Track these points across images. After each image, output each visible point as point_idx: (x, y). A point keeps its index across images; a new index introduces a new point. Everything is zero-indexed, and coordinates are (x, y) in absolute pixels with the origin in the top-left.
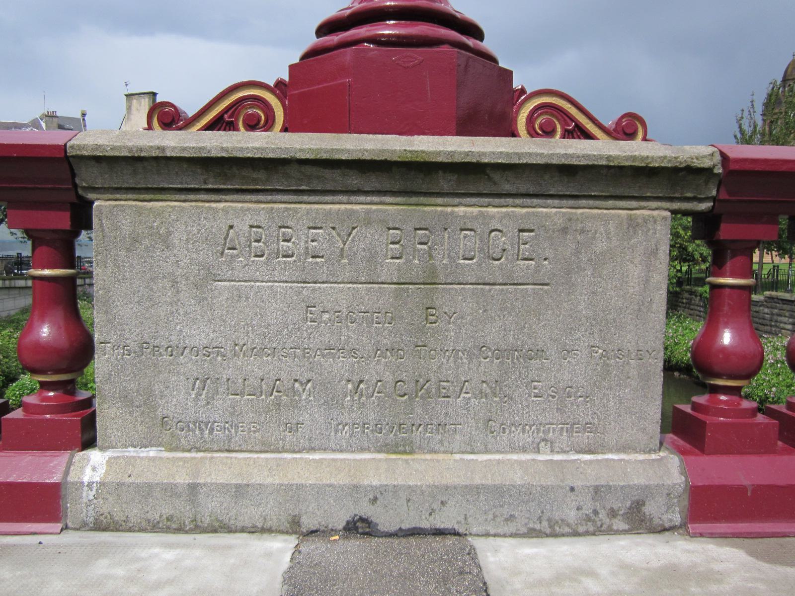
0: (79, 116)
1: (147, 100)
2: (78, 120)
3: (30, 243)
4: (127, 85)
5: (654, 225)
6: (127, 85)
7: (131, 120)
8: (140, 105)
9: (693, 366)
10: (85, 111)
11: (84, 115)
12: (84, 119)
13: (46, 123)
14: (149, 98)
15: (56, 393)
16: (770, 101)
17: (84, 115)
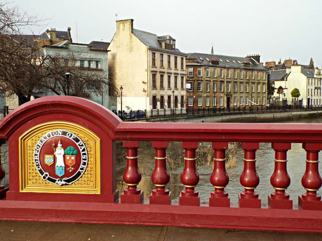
0: (66, 30)
3: (63, 149)
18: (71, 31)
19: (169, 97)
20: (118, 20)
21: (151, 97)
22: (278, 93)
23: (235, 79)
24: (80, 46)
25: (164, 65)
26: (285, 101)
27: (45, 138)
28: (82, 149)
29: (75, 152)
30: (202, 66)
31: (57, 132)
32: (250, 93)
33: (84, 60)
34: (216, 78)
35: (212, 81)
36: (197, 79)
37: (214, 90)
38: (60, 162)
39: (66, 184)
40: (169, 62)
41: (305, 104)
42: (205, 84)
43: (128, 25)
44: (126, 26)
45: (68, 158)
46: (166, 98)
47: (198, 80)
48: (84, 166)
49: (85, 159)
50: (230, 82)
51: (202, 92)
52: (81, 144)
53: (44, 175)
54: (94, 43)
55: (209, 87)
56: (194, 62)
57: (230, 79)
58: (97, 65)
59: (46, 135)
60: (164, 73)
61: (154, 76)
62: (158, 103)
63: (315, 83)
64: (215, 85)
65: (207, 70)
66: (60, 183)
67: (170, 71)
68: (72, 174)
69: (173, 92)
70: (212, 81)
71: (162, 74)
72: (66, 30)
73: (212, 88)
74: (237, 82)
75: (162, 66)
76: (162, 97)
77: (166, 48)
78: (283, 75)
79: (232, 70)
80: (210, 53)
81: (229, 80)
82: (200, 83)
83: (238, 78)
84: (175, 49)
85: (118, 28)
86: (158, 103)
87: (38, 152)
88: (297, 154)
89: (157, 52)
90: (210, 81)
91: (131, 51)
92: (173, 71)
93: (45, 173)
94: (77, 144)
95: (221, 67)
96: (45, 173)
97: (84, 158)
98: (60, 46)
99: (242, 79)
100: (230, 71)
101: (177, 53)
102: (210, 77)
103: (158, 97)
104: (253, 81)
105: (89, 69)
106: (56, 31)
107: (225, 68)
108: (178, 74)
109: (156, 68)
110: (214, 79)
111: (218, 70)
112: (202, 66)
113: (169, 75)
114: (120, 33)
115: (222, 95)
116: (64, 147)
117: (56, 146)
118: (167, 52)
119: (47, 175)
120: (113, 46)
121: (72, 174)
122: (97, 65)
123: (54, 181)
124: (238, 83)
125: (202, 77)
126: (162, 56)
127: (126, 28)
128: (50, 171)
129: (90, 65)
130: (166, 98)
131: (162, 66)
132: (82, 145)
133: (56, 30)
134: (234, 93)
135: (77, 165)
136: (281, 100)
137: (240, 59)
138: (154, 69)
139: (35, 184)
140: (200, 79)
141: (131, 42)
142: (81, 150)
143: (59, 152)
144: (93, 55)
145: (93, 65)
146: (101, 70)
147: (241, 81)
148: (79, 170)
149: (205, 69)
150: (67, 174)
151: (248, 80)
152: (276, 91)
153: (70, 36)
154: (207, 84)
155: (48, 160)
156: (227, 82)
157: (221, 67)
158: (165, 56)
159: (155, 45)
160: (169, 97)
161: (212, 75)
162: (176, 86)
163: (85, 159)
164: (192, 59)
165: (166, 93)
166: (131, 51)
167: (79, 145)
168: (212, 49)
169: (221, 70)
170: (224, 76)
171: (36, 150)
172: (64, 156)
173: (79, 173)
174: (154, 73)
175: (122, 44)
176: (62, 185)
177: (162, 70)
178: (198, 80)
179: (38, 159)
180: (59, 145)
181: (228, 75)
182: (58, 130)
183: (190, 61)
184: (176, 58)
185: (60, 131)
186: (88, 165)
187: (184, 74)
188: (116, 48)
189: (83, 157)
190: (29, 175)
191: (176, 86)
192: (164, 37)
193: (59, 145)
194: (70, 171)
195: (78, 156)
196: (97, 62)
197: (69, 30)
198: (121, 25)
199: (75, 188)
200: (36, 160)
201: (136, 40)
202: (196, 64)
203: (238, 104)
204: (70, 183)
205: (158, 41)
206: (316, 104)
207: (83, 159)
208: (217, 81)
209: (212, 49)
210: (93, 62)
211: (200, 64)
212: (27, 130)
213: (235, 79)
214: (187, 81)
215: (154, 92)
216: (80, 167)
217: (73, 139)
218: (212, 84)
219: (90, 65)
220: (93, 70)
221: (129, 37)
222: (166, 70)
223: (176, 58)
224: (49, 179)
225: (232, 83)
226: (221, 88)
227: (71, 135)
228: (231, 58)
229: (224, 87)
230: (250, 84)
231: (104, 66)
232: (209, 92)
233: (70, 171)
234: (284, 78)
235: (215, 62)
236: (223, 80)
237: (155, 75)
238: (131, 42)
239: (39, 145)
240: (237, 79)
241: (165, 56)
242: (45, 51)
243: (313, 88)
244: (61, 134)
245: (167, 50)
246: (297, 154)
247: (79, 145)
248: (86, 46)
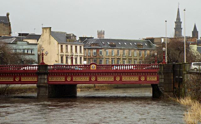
0: (6, 15)
12: (8, 17)
18: (9, 16)
23: (129, 57)
30: (103, 48)
33: (25, 50)
35: (110, 58)
36: (99, 57)
42: (105, 61)
43: (48, 30)
47: (99, 58)
50: (125, 59)
56: (97, 46)
58: (32, 52)
61: (62, 58)
65: (107, 51)
70: (110, 58)
72: (6, 15)
75: (67, 52)
79: (127, 50)
81: (125, 58)
82: (101, 60)
85: (43, 32)
88: (37, 67)
90: (109, 58)
91: (50, 44)
95: (117, 49)
99: (135, 57)
102: (108, 56)
105: (28, 54)
108: (77, 56)
110: (112, 57)
111: (115, 51)
112: (103, 48)
118: (70, 44)
120: (41, 41)
122: (32, 52)
124: (133, 60)
125: (103, 56)
127: (47, 32)
129: (28, 51)
138: (62, 54)
140: (101, 57)
141: (50, 39)
145: (29, 52)
146: (34, 54)
147: (135, 58)
149: (105, 50)
151: (142, 57)
153: (9, 20)
156: (123, 59)
159: (64, 39)
161: (110, 54)
164: (95, 44)
166: (50, 44)
168: (178, 9)
170: (120, 55)
174: (62, 56)
177: (67, 54)
178: (99, 58)
183: (94, 45)
187: (82, 56)
188: (42, 42)
192: (70, 35)
197: (8, 15)
198: (45, 30)
201: (52, 39)
202: (98, 47)
205: (67, 37)
208: (115, 58)
210: (30, 50)
211: (101, 47)
213: (129, 57)
214: (85, 59)
219: (28, 51)
220: (29, 54)
221: (49, 37)
222: (65, 54)
225: (127, 60)
231: (35, 52)
235: (113, 44)
236: (119, 57)
237: (62, 57)
238: (50, 39)
240: (131, 57)
245: (70, 43)
246: (37, 67)
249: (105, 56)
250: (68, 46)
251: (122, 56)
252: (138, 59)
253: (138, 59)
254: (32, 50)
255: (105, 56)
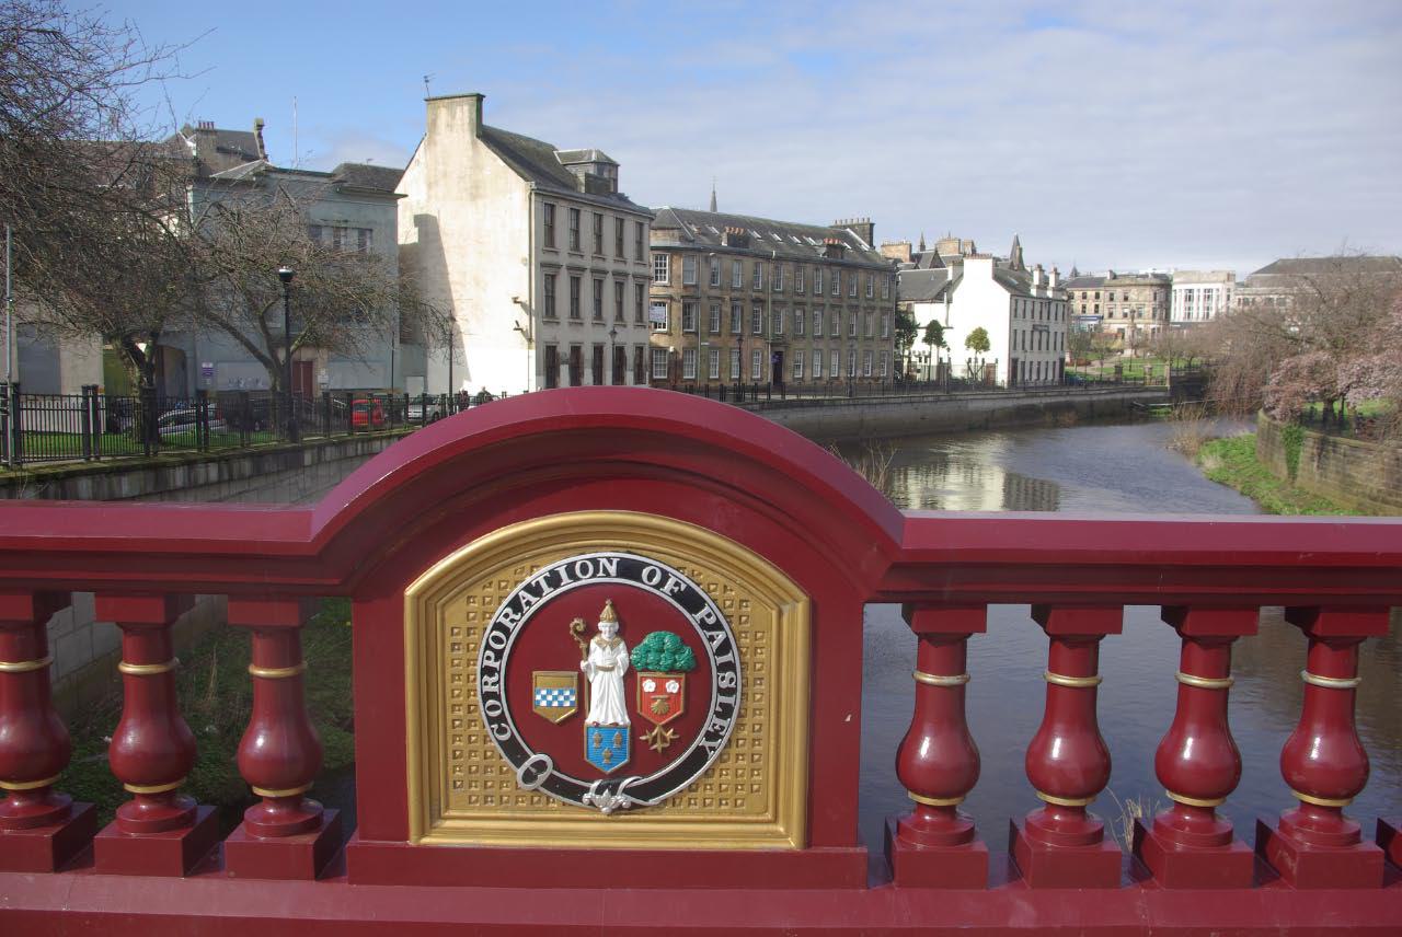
0: (252, 129)
1: (466, 108)
2: (249, 135)
4: (427, 81)
5: (991, 261)
6: (427, 81)
7: (435, 144)
8: (453, 117)
9: (324, 827)
10: (262, 120)
11: (260, 127)
12: (260, 136)
13: (197, 141)
14: (471, 105)
15: (152, 806)
16: (1382, 269)
17: (260, 127)
19: (598, 350)
20: (432, 96)
21: (543, 347)
22: (927, 340)
23: (798, 295)
24: (304, 178)
25: (582, 247)
26: (944, 368)
27: (535, 590)
28: (529, 597)
29: (684, 658)
31: (595, 562)
32: (844, 338)
34: (741, 290)
35: (727, 298)
37: (733, 328)
38: (607, 708)
39: (634, 806)
40: (599, 236)
41: (1002, 376)
43: (464, 113)
44: (459, 114)
45: (649, 686)
46: (588, 354)
48: (724, 723)
49: (730, 692)
51: (696, 333)
52: (711, 621)
53: (527, 764)
54: (352, 169)
55: (717, 317)
57: (783, 293)
59: (539, 576)
60: (584, 269)
62: (564, 371)
63: (1033, 312)
64: (738, 312)
66: (609, 801)
67: (601, 265)
68: (662, 757)
69: (614, 333)
70: (727, 298)
71: (598, 276)
72: (252, 129)
73: (727, 320)
74: (804, 304)
75: (576, 246)
76: (576, 350)
77: (587, 191)
78: (941, 285)
80: (707, 209)
81: (780, 297)
83: (810, 294)
84: (615, 193)
86: (564, 371)
87: (499, 655)
89: (586, 208)
90: (722, 299)
92: (610, 265)
93: (534, 758)
94: (693, 619)
95: (756, 256)
96: (534, 758)
97: (724, 684)
98: (239, 177)
99: (818, 295)
100: (787, 270)
101: (623, 206)
103: (564, 350)
104: (854, 302)
106: (216, 132)
107: (768, 258)
109: (625, 262)
113: (576, 274)
114: (438, 138)
115: (759, 344)
116: (629, 633)
117: (591, 631)
119: (540, 766)
121: (662, 757)
123: (575, 793)
126: (622, 226)
128: (561, 754)
130: (588, 354)
131: (576, 246)
132: (718, 626)
133: (217, 127)
134: (796, 338)
135: (690, 715)
136: (934, 362)
137: (817, 233)
139: (482, 813)
142: (711, 647)
143: (605, 659)
144: (335, 211)
147: (816, 300)
148: (700, 741)
150: (641, 757)
151: (840, 297)
152: (922, 333)
153: (262, 147)
154: (712, 308)
155: (551, 696)
156: (774, 302)
157: (756, 256)
158: (587, 218)
160: (598, 350)
162: (620, 316)
163: (730, 692)
165: (589, 336)
167: (703, 624)
168: (714, 193)
169: (757, 265)
170: (765, 284)
171: (488, 647)
172: (630, 680)
173: (700, 756)
175: (445, 175)
176: (619, 809)
179: (501, 689)
180: (605, 627)
181: (779, 280)
182: (601, 555)
184: (621, 222)
185: (609, 558)
186: (740, 716)
189: (723, 680)
190: (451, 762)
191: (620, 316)
193: (605, 627)
194: (658, 746)
195: (697, 677)
196: (362, 232)
199: (678, 827)
200: (486, 696)
201: (492, 162)
203: (808, 372)
204: (652, 802)
206: (1034, 377)
207: (722, 691)
209: (715, 198)
212: (434, 562)
213: (798, 295)
215: (550, 334)
216: (707, 727)
217: (674, 595)
218: (727, 309)
223: (621, 222)
224: (552, 784)
226: (756, 323)
227: (665, 576)
228: (785, 230)
229: (764, 319)
230: (845, 311)
232: (719, 334)
233: (658, 746)
234: (942, 293)
238: (477, 167)
239: (506, 622)
240: (803, 295)
241: (587, 218)
242: (190, 198)
243: (1029, 329)
244: (612, 569)
247: (703, 624)
248: (325, 180)
249: (706, 288)
250: (582, 213)
251: (773, 288)
252: (828, 306)
253: (828, 306)
254: (362, 232)
255: (706, 288)
